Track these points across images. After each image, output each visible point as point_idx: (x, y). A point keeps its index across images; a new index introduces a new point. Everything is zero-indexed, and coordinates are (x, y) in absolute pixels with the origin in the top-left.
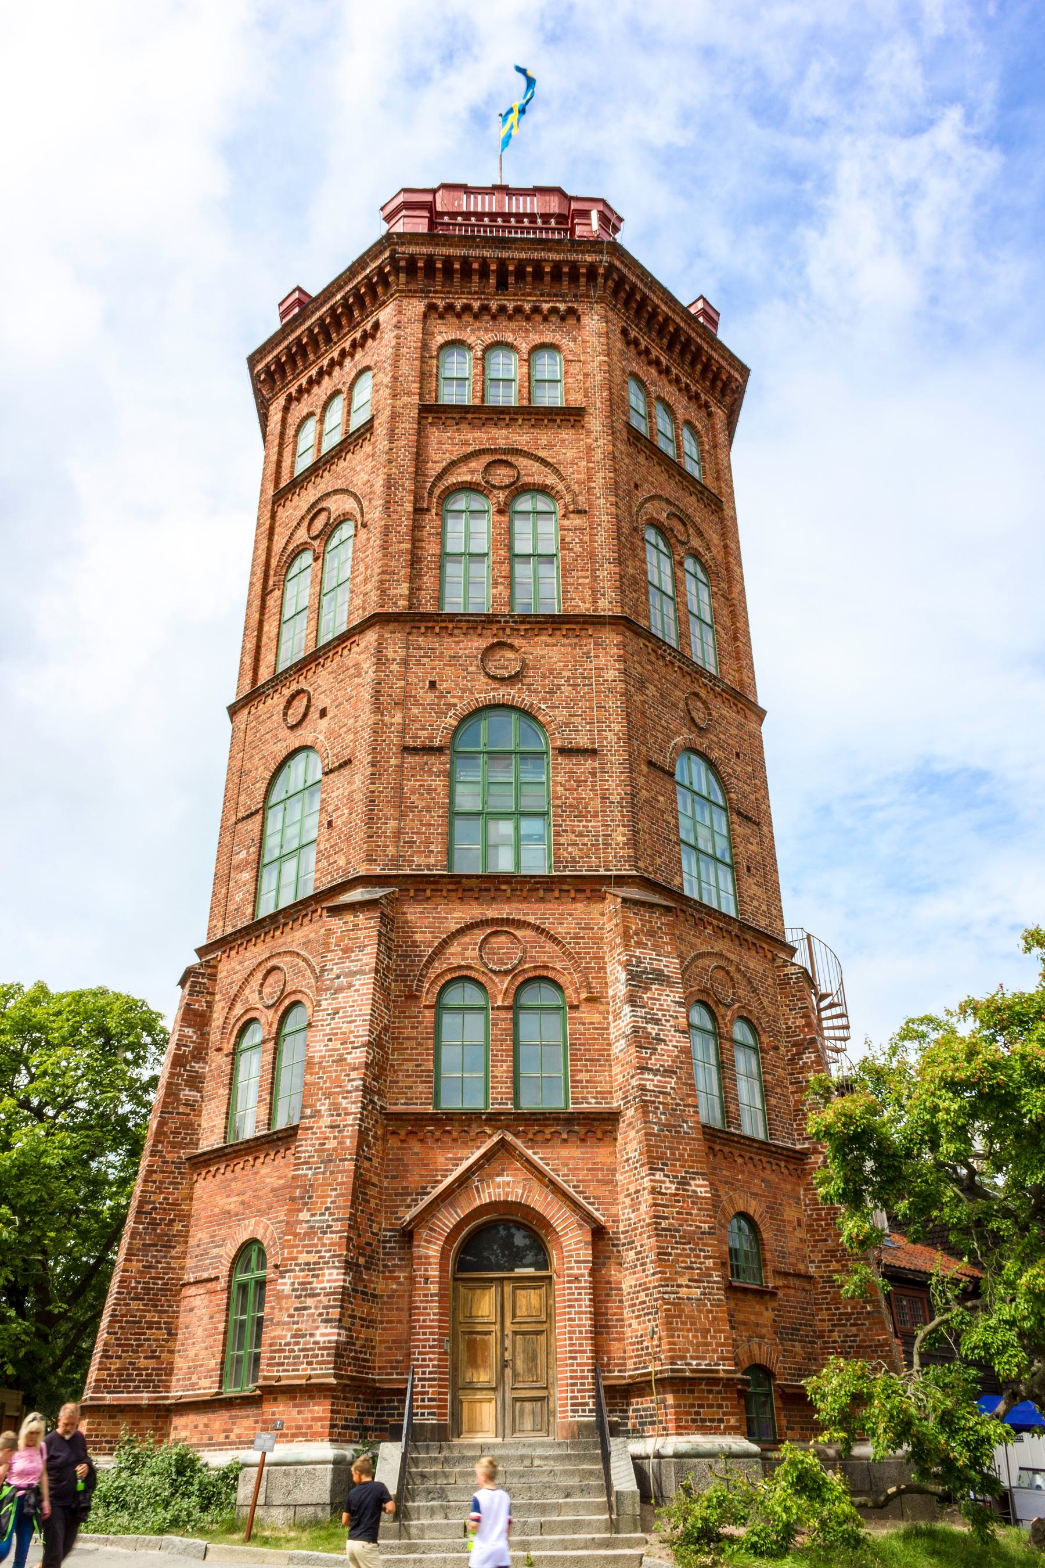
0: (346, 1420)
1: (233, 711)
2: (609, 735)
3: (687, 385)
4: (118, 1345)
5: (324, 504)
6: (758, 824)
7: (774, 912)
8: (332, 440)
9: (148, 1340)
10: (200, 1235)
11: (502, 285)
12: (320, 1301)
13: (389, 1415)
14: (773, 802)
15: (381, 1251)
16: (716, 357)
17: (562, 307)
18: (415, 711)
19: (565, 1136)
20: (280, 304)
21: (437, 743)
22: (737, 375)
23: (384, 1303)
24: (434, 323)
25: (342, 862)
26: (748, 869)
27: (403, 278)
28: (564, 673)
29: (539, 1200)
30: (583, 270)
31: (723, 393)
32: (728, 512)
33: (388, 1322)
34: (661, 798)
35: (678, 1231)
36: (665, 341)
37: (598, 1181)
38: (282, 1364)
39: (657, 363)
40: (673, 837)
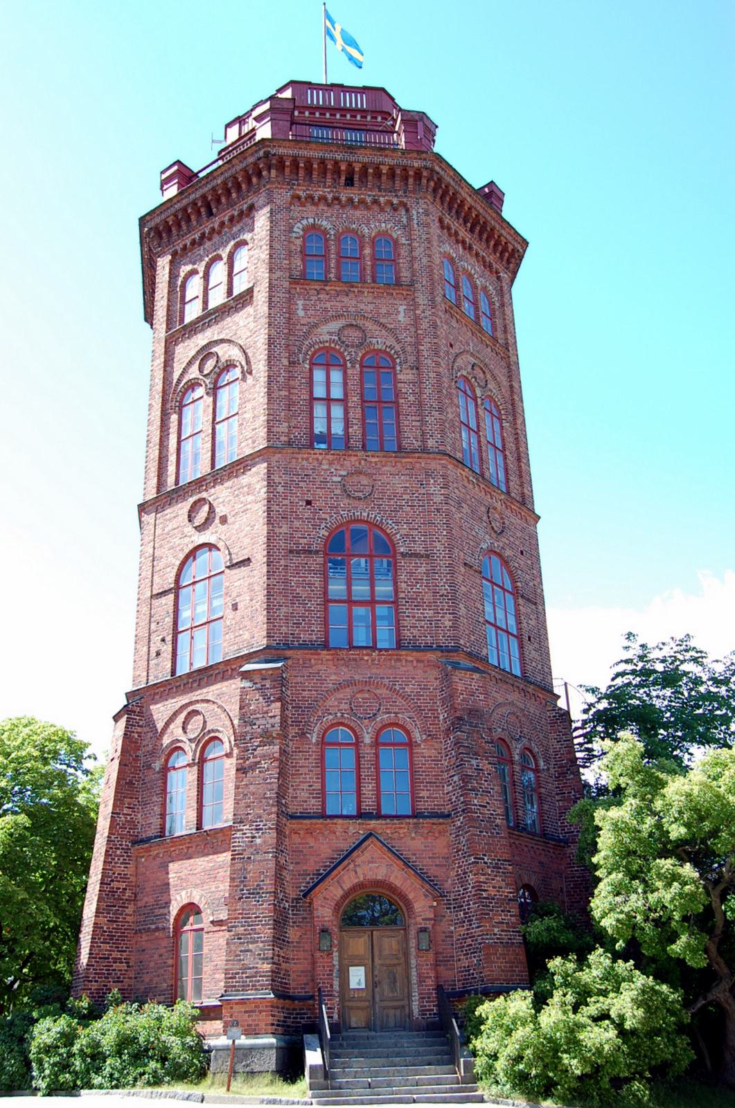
0: (278, 1021)
1: (142, 508)
2: (437, 544)
3: (483, 257)
4: (95, 974)
5: (213, 350)
6: (535, 604)
7: (546, 670)
8: (217, 298)
9: (114, 970)
10: (146, 899)
11: (350, 182)
12: (258, 946)
13: (301, 1018)
14: (545, 587)
15: (290, 912)
16: (505, 234)
17: (395, 201)
18: (297, 524)
19: (413, 835)
20: (162, 173)
21: (314, 548)
22: (519, 248)
23: (294, 947)
24: (296, 210)
25: (247, 636)
26: (529, 638)
27: (273, 173)
28: (404, 497)
29: (398, 877)
30: (411, 173)
31: (508, 262)
32: (513, 359)
33: (297, 959)
34: (474, 591)
35: (494, 899)
36: (469, 225)
37: (436, 866)
38: (235, 986)
39: (463, 242)
40: (481, 620)
